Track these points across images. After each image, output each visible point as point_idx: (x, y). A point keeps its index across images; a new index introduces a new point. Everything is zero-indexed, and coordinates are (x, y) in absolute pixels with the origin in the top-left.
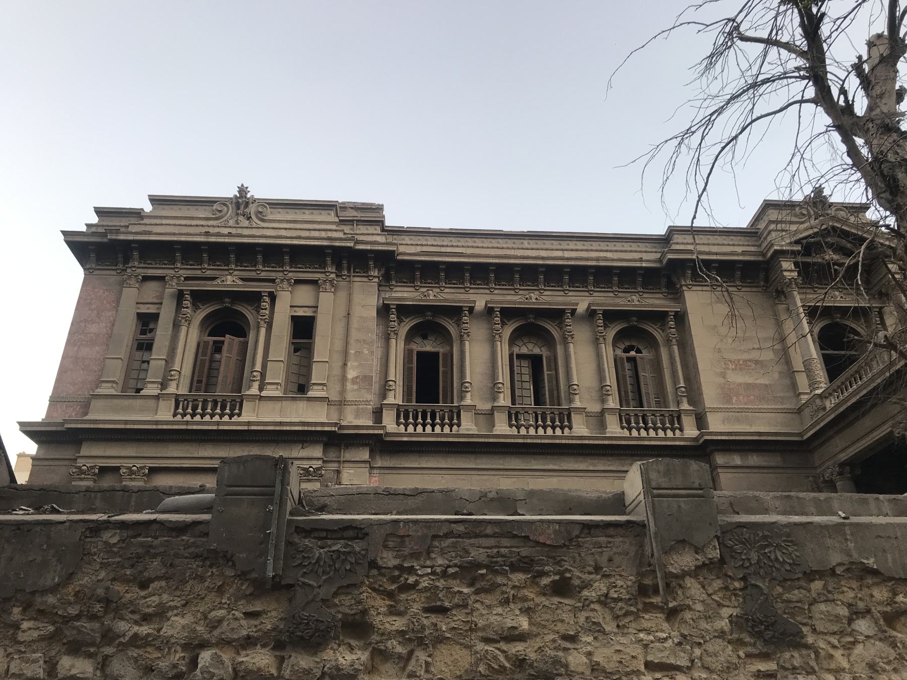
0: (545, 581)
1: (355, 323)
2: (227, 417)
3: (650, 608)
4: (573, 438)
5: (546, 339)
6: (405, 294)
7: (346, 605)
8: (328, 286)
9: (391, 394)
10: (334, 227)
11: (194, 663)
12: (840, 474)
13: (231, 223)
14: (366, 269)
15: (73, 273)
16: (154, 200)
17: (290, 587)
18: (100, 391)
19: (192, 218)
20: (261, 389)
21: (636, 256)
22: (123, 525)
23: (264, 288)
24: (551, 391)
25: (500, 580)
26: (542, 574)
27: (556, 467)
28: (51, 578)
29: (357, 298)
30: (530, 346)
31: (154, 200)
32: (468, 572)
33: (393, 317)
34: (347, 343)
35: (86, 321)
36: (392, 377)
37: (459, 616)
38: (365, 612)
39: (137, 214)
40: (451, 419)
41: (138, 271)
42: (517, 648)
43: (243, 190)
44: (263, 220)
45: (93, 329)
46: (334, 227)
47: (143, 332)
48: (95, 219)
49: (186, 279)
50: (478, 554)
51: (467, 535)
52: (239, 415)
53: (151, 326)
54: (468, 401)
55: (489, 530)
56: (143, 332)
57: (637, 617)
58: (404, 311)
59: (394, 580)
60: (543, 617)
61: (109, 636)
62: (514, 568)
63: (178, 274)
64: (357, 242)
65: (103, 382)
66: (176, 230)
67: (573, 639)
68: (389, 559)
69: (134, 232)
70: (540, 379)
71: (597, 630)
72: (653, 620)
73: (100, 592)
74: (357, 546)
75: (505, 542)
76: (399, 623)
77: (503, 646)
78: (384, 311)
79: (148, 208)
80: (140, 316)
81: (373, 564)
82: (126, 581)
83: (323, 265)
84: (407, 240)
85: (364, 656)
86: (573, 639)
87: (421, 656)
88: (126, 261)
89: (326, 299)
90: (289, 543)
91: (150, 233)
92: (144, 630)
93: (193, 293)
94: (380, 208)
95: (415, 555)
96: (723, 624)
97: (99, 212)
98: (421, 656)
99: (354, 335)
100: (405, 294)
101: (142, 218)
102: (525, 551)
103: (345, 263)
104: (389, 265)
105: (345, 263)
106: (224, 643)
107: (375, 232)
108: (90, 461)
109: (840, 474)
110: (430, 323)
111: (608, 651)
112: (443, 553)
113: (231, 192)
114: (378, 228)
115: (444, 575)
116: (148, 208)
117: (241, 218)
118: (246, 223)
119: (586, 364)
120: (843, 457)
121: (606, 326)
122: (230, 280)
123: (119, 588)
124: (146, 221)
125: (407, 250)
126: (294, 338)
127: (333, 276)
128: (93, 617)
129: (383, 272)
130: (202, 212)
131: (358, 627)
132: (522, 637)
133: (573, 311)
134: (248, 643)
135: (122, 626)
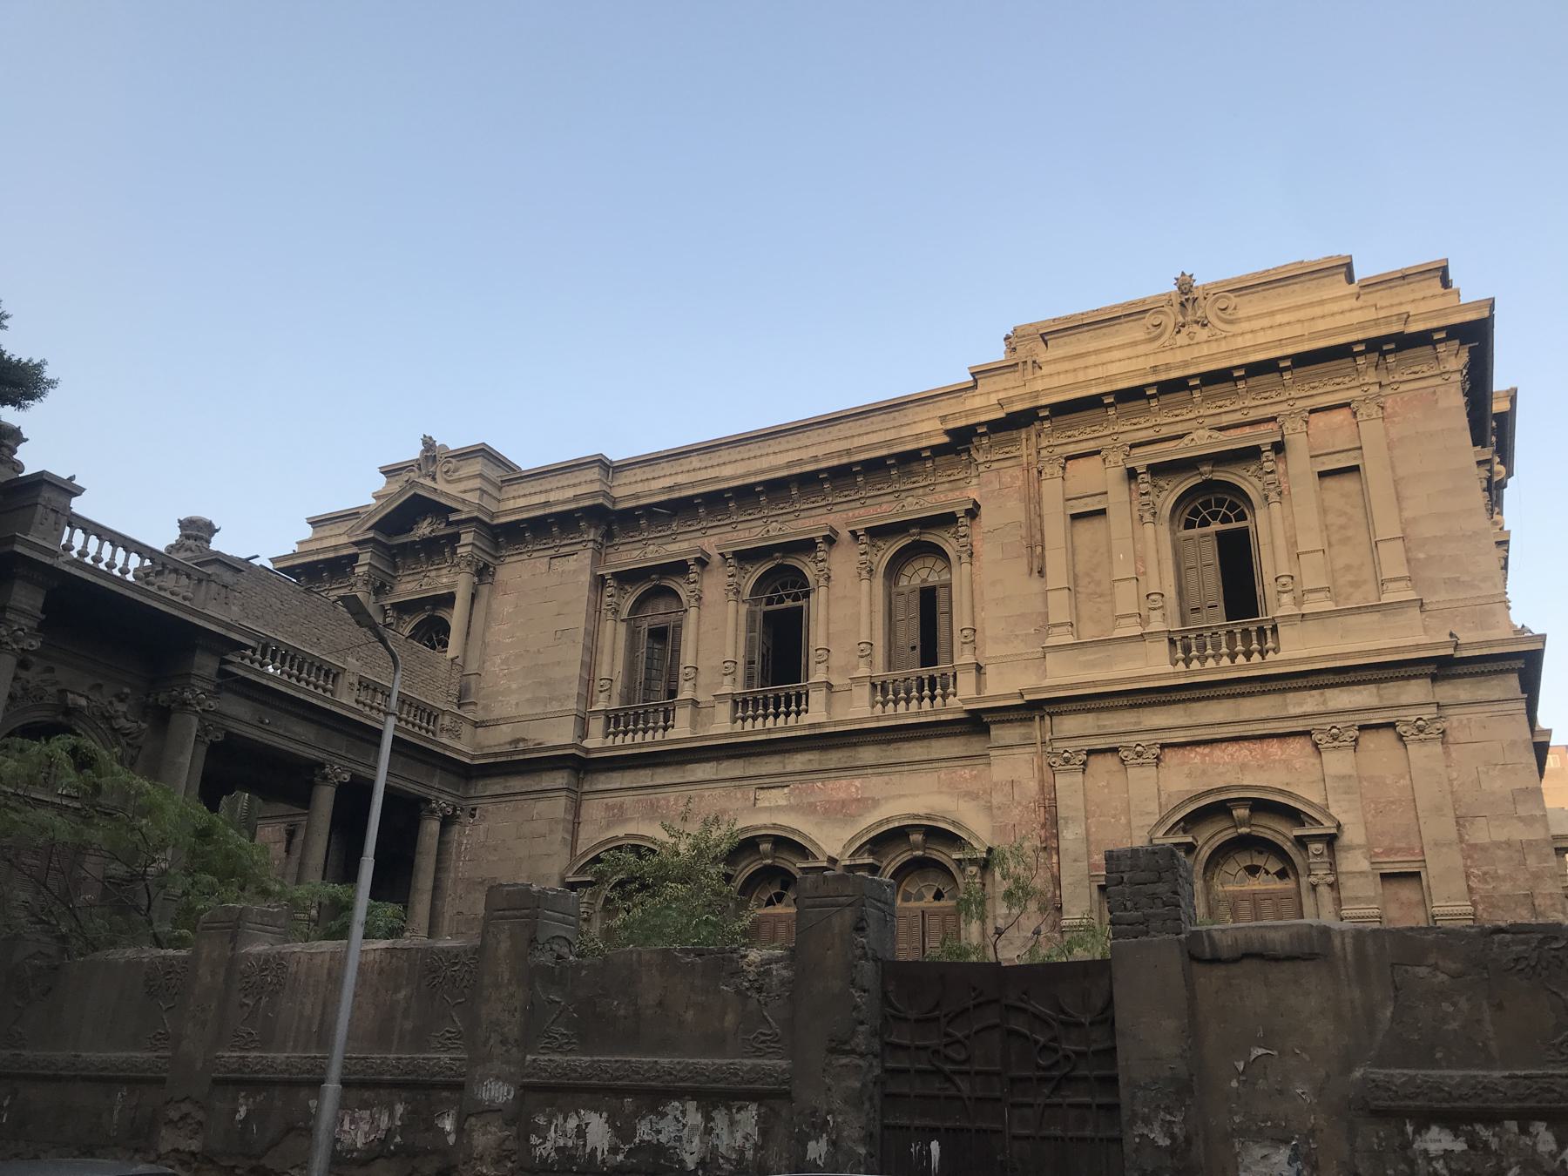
2: (1210, 660)
6: (632, 554)
10: (1346, 305)
18: (1051, 641)
19: (1322, 302)
20: (1298, 602)
21: (570, 493)
23: (1263, 436)
36: (604, 671)
41: (1122, 437)
43: (428, 443)
44: (1231, 322)
49: (1132, 446)
52: (1276, 650)
58: (626, 578)
65: (1055, 626)
66: (1297, 330)
70: (781, 653)
100: (632, 554)
107: (1429, 293)
108: (1342, 718)
110: (657, 585)
113: (414, 452)
118: (1203, 334)
119: (848, 615)
122: (1200, 430)
126: (1246, 530)
129: (603, 528)
130: (1135, 331)
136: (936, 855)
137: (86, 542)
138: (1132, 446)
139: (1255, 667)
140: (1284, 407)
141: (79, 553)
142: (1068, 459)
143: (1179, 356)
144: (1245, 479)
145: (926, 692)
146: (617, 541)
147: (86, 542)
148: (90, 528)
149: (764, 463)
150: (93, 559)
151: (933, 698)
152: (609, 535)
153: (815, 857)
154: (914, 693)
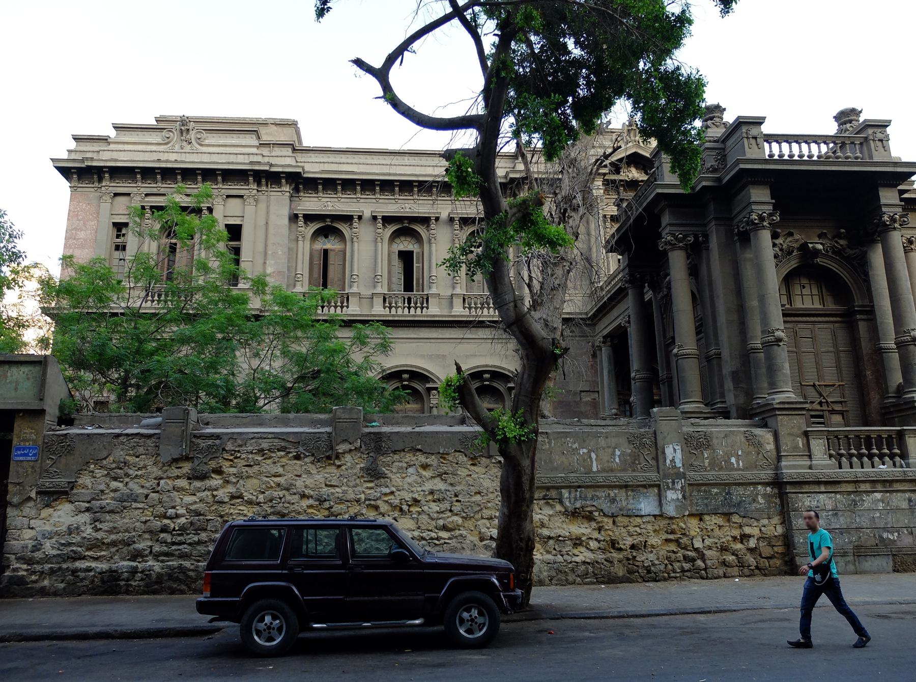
0: (291, 455)
1: (271, 230)
3: (330, 464)
4: (428, 316)
5: (415, 236)
6: (312, 203)
7: (213, 464)
8: (252, 200)
9: (298, 284)
10: (254, 150)
11: (158, 484)
12: (604, 342)
13: (177, 148)
14: (279, 184)
15: (63, 184)
16: (117, 127)
17: (192, 458)
22: (127, 435)
24: (418, 280)
25: (273, 455)
26: (289, 452)
27: (416, 336)
28: (105, 454)
29: (273, 208)
30: (406, 243)
31: (117, 127)
32: (261, 451)
33: (301, 223)
34: (266, 246)
35: (76, 229)
37: (256, 468)
38: (221, 467)
39: (105, 140)
40: (342, 303)
41: (110, 189)
42: (277, 479)
44: (201, 145)
45: (82, 235)
46: (254, 150)
47: (118, 236)
48: (73, 145)
49: (147, 195)
50: (265, 445)
51: (261, 438)
53: (124, 231)
54: (355, 289)
55: (270, 436)
56: (118, 236)
57: (325, 468)
58: (309, 218)
59: (232, 455)
60: (288, 468)
61: (127, 475)
62: (279, 450)
63: (139, 189)
64: (271, 165)
67: (299, 476)
68: (229, 447)
69: (105, 157)
71: (309, 473)
72: (332, 469)
73: (122, 460)
74: (218, 442)
75: (277, 440)
76: (233, 470)
77: (273, 478)
78: (294, 218)
79: (112, 133)
80: (115, 224)
81: (224, 449)
82: (130, 455)
83: (247, 182)
84: (313, 157)
85: (220, 482)
86: (299, 476)
87: (241, 482)
88: (100, 180)
89: (250, 210)
90: (191, 442)
91: (116, 160)
92: (140, 473)
93: (152, 207)
94: (293, 125)
95: (240, 446)
96: (357, 470)
97: (77, 139)
98: (241, 482)
99: (272, 240)
100: (312, 203)
101: (109, 143)
102: (283, 444)
103: (264, 181)
104: (300, 183)
105: (264, 181)
106: (169, 478)
109: (604, 342)
111: (312, 481)
112: (251, 445)
114: (290, 150)
115: (252, 453)
116: (112, 133)
117: (184, 144)
118: (188, 148)
120: (605, 332)
121: (461, 228)
123: (127, 457)
124: (112, 147)
125: (313, 168)
127: (255, 192)
128: (121, 469)
129: (293, 186)
131: (219, 471)
132: (280, 476)
133: (437, 219)
134: (178, 477)
135: (131, 472)
136: (495, 384)
137: (790, 148)
138: (147, 195)
139: (416, 314)
140: (135, 189)
141: (808, 156)
142: (228, 196)
143: (173, 157)
144: (343, 227)
145: (406, 305)
146: (302, 194)
147: (790, 148)
148: (769, 138)
149: (418, 171)
150: (808, 156)
151: (409, 308)
152: (297, 190)
153: (434, 382)
154: (419, 305)
